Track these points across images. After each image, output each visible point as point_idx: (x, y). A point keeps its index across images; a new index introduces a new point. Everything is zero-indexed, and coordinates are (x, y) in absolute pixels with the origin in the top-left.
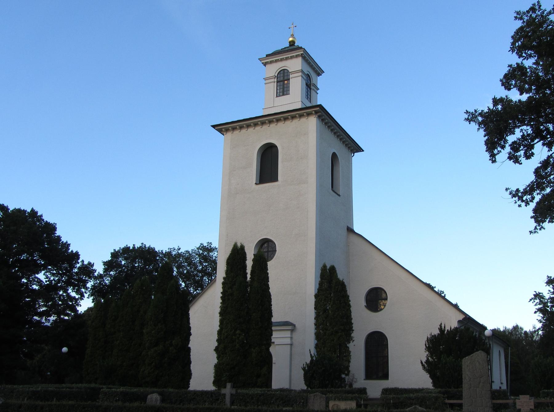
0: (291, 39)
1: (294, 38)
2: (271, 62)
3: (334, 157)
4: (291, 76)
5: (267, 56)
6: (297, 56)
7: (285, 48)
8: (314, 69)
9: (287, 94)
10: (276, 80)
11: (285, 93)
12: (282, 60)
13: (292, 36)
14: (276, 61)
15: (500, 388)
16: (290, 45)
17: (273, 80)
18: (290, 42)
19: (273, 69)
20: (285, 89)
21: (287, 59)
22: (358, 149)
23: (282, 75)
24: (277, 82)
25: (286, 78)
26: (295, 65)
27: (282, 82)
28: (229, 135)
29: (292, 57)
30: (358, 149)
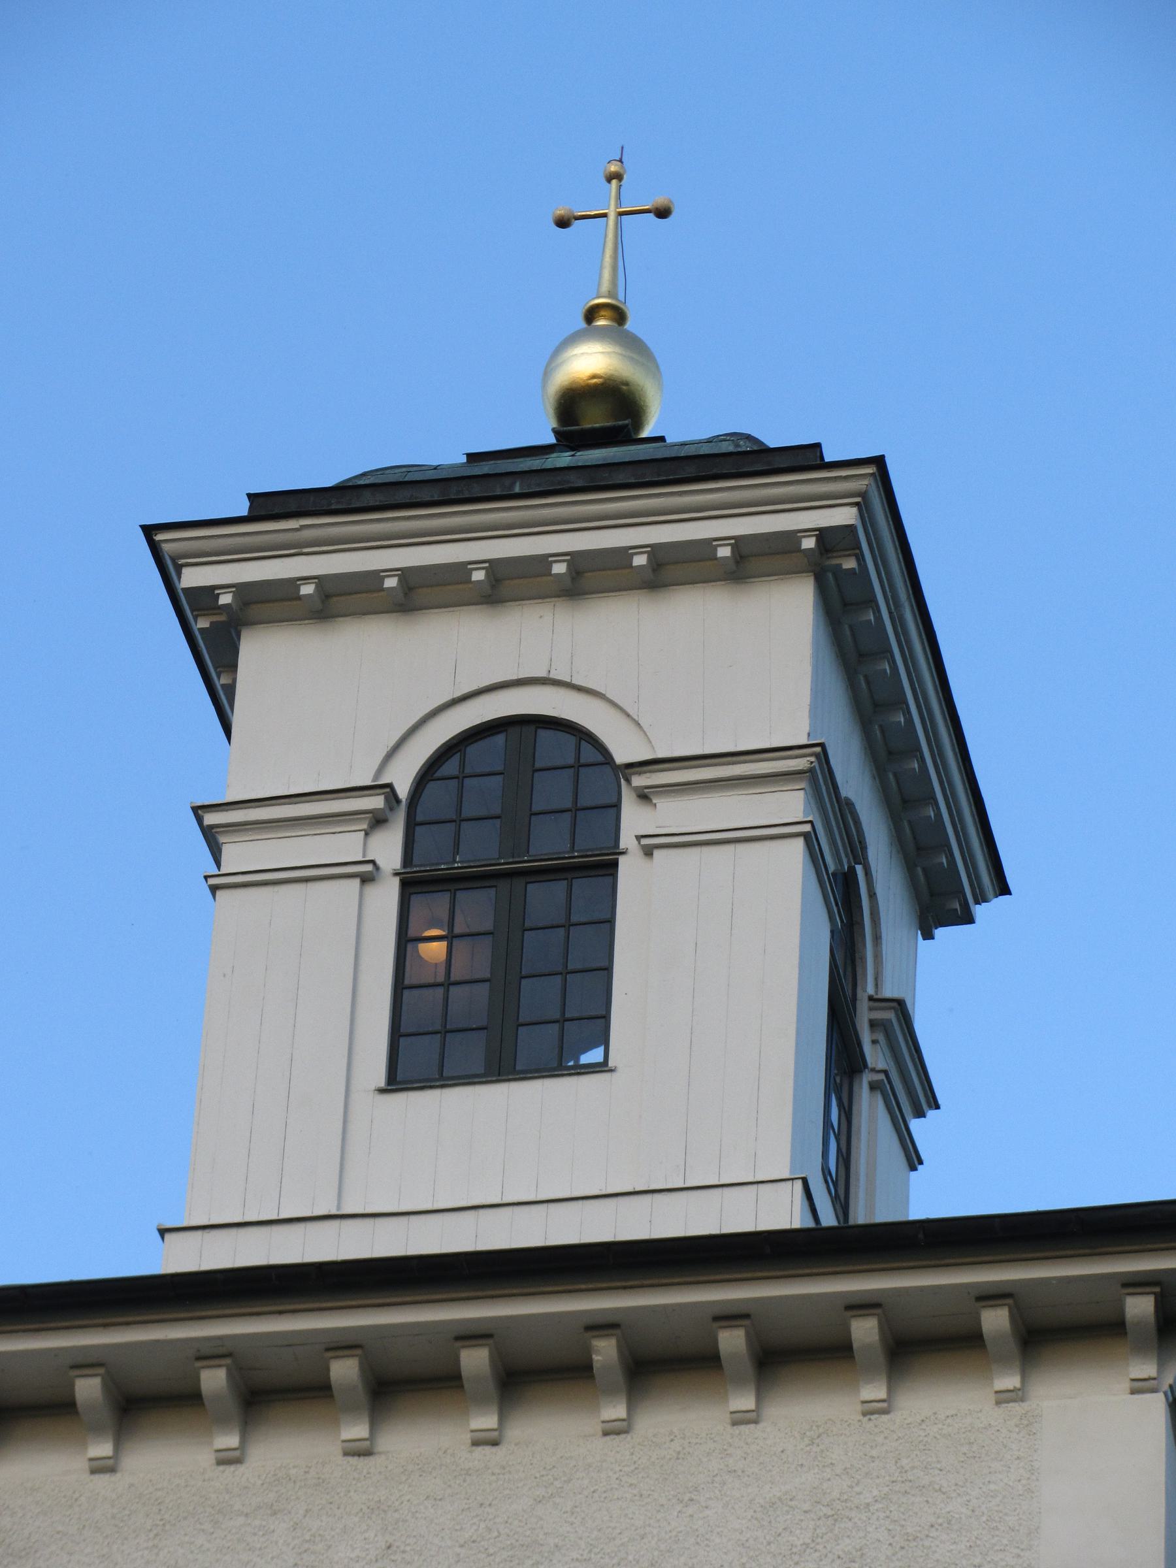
0: (590, 361)
1: (634, 346)
4: (634, 820)
5: (267, 506)
6: (750, 562)
7: (364, 474)
9: (560, 1065)
10: (388, 849)
11: (534, 1042)
12: (504, 586)
13: (607, 317)
14: (416, 594)
16: (571, 433)
17: (345, 846)
18: (571, 402)
19: (354, 704)
20: (537, 996)
21: (587, 579)
22: (938, 1107)
23: (485, 794)
24: (413, 884)
25: (549, 841)
26: (712, 676)
27: (504, 882)
29: (668, 571)
30: (938, 1107)
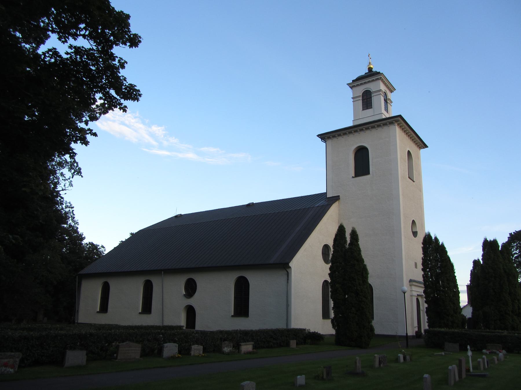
2: (358, 85)
3: (409, 152)
5: (353, 81)
8: (388, 88)
12: (365, 83)
14: (362, 84)
15: (191, 289)
19: (360, 90)
21: (369, 82)
22: (426, 146)
28: (329, 142)
30: (426, 146)
